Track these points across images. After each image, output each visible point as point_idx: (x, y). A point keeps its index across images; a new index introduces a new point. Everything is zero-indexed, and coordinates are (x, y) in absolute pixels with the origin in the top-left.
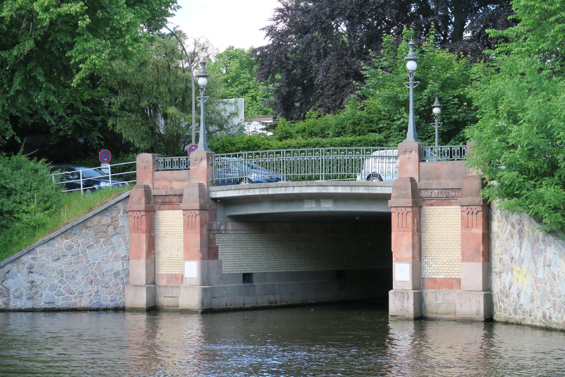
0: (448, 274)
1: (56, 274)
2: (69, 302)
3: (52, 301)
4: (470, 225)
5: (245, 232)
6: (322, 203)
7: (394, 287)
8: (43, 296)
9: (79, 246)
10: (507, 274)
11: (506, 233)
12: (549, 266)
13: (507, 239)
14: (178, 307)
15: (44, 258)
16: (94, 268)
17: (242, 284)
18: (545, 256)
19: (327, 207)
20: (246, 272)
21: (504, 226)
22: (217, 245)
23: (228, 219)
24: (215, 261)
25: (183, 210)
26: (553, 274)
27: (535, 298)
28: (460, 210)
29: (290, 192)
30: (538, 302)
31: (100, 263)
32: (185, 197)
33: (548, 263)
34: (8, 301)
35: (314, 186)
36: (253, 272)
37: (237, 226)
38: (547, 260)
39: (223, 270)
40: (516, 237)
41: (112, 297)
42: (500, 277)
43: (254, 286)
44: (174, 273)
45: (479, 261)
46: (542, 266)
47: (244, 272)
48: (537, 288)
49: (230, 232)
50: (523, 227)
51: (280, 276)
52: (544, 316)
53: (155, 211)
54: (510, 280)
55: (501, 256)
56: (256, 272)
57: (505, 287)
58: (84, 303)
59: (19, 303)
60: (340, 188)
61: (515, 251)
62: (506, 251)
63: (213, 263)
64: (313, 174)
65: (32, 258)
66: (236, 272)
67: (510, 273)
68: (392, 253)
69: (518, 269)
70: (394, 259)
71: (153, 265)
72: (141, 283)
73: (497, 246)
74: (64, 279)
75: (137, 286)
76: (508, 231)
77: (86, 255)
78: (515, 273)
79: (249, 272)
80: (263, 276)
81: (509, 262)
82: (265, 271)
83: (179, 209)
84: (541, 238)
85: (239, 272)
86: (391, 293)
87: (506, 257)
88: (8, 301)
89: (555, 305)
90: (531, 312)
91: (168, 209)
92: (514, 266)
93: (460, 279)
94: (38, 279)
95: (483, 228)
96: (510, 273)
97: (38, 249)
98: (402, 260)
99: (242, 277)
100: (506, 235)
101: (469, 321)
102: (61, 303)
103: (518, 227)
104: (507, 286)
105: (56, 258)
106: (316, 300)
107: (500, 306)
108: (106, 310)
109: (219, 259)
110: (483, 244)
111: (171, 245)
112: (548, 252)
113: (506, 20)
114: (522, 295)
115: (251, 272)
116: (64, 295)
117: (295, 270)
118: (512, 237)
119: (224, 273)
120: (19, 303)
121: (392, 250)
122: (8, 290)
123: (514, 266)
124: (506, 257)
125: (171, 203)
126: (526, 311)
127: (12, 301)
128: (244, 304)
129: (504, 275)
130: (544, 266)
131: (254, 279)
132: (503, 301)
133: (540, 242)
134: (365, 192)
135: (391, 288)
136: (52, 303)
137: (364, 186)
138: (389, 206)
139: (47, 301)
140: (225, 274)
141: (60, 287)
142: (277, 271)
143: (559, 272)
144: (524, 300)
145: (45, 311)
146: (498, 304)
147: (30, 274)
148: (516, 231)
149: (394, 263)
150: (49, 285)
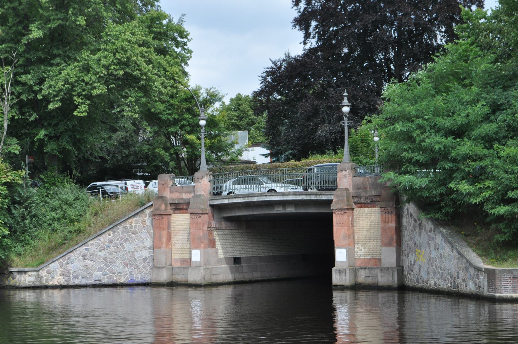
0: (373, 255)
1: (102, 260)
2: (112, 279)
3: (100, 279)
4: (387, 221)
5: (235, 228)
6: (287, 208)
7: (336, 265)
8: (94, 276)
9: (118, 240)
10: (412, 255)
11: (411, 227)
12: (438, 249)
13: (412, 231)
14: (188, 282)
15: (94, 249)
16: (129, 255)
17: (233, 265)
18: (436, 242)
19: (290, 210)
20: (236, 256)
21: (409, 221)
22: (214, 237)
23: (222, 219)
24: (213, 249)
25: (190, 214)
26: (441, 254)
27: (430, 271)
28: (379, 210)
29: (264, 200)
30: (432, 275)
31: (133, 251)
32: (191, 204)
33: (437, 247)
34: (69, 280)
35: (241, 197)
36: (241, 256)
37: (229, 224)
38: (437, 245)
39: (219, 255)
40: (417, 229)
41: (142, 275)
42: (408, 257)
43: (242, 266)
44: (185, 258)
45: (394, 246)
46: (434, 249)
47: (234, 257)
48: (431, 264)
49: (224, 228)
50: (422, 221)
51: (260, 259)
52: (435, 285)
53: (354, 209)
54: (414, 259)
55: (408, 243)
56: (243, 256)
57: (411, 264)
58: (123, 280)
59: (77, 281)
60: (314, 196)
61: (417, 240)
62: (411, 239)
63: (211, 250)
64: (329, 186)
65: (86, 249)
66: (229, 257)
67: (414, 255)
68: (334, 241)
69: (419, 251)
70: (335, 246)
71: (170, 252)
72: (162, 265)
73: (405, 236)
74: (108, 263)
75: (159, 268)
76: (412, 225)
77: (124, 247)
78: (417, 254)
79: (238, 256)
80: (249, 259)
81: (413, 246)
82: (250, 256)
83: (187, 213)
84: (433, 229)
85: (231, 257)
86: (334, 269)
87: (411, 243)
88: (69, 280)
89: (442, 276)
90: (427, 282)
91: (180, 213)
92: (417, 250)
93: (381, 259)
94: (90, 264)
95: (396, 223)
96: (414, 255)
97: (90, 243)
98: (340, 247)
99: (233, 260)
100: (411, 228)
101: (387, 289)
102: (106, 280)
103: (418, 222)
104: (412, 263)
105: (102, 249)
106: (262, 277)
107: (408, 277)
108: (122, 285)
109: (216, 247)
110: (396, 234)
111: (182, 238)
112: (437, 239)
113: (372, 73)
114: (422, 269)
115: (240, 256)
116: (108, 274)
117: (272, 255)
118: (415, 229)
119: (220, 257)
120: (77, 281)
121: (334, 239)
122: (69, 271)
123: (417, 250)
124: (411, 243)
125: (182, 209)
126: (424, 280)
127: (71, 279)
128: (279, 276)
129: (410, 256)
130: (435, 249)
131: (242, 261)
132: (410, 275)
133: (432, 232)
134: (315, 199)
135: (334, 266)
136: (100, 280)
137: (314, 195)
138: (331, 208)
139: (97, 279)
140: (221, 258)
141: (106, 269)
142: (258, 255)
143: (444, 253)
144: (423, 274)
145: (94, 286)
146: (407, 276)
147: (84, 260)
148: (417, 224)
149: (335, 248)
150: (98, 267)
